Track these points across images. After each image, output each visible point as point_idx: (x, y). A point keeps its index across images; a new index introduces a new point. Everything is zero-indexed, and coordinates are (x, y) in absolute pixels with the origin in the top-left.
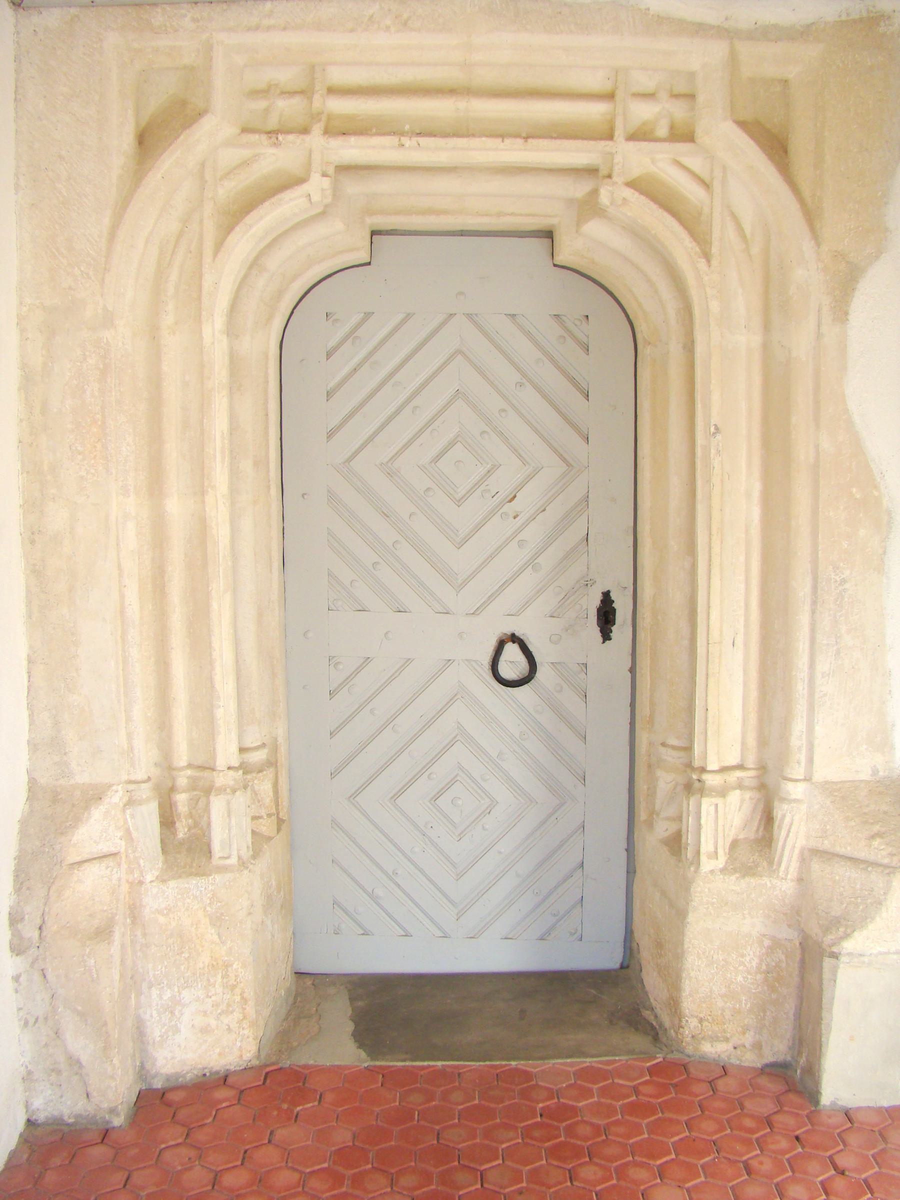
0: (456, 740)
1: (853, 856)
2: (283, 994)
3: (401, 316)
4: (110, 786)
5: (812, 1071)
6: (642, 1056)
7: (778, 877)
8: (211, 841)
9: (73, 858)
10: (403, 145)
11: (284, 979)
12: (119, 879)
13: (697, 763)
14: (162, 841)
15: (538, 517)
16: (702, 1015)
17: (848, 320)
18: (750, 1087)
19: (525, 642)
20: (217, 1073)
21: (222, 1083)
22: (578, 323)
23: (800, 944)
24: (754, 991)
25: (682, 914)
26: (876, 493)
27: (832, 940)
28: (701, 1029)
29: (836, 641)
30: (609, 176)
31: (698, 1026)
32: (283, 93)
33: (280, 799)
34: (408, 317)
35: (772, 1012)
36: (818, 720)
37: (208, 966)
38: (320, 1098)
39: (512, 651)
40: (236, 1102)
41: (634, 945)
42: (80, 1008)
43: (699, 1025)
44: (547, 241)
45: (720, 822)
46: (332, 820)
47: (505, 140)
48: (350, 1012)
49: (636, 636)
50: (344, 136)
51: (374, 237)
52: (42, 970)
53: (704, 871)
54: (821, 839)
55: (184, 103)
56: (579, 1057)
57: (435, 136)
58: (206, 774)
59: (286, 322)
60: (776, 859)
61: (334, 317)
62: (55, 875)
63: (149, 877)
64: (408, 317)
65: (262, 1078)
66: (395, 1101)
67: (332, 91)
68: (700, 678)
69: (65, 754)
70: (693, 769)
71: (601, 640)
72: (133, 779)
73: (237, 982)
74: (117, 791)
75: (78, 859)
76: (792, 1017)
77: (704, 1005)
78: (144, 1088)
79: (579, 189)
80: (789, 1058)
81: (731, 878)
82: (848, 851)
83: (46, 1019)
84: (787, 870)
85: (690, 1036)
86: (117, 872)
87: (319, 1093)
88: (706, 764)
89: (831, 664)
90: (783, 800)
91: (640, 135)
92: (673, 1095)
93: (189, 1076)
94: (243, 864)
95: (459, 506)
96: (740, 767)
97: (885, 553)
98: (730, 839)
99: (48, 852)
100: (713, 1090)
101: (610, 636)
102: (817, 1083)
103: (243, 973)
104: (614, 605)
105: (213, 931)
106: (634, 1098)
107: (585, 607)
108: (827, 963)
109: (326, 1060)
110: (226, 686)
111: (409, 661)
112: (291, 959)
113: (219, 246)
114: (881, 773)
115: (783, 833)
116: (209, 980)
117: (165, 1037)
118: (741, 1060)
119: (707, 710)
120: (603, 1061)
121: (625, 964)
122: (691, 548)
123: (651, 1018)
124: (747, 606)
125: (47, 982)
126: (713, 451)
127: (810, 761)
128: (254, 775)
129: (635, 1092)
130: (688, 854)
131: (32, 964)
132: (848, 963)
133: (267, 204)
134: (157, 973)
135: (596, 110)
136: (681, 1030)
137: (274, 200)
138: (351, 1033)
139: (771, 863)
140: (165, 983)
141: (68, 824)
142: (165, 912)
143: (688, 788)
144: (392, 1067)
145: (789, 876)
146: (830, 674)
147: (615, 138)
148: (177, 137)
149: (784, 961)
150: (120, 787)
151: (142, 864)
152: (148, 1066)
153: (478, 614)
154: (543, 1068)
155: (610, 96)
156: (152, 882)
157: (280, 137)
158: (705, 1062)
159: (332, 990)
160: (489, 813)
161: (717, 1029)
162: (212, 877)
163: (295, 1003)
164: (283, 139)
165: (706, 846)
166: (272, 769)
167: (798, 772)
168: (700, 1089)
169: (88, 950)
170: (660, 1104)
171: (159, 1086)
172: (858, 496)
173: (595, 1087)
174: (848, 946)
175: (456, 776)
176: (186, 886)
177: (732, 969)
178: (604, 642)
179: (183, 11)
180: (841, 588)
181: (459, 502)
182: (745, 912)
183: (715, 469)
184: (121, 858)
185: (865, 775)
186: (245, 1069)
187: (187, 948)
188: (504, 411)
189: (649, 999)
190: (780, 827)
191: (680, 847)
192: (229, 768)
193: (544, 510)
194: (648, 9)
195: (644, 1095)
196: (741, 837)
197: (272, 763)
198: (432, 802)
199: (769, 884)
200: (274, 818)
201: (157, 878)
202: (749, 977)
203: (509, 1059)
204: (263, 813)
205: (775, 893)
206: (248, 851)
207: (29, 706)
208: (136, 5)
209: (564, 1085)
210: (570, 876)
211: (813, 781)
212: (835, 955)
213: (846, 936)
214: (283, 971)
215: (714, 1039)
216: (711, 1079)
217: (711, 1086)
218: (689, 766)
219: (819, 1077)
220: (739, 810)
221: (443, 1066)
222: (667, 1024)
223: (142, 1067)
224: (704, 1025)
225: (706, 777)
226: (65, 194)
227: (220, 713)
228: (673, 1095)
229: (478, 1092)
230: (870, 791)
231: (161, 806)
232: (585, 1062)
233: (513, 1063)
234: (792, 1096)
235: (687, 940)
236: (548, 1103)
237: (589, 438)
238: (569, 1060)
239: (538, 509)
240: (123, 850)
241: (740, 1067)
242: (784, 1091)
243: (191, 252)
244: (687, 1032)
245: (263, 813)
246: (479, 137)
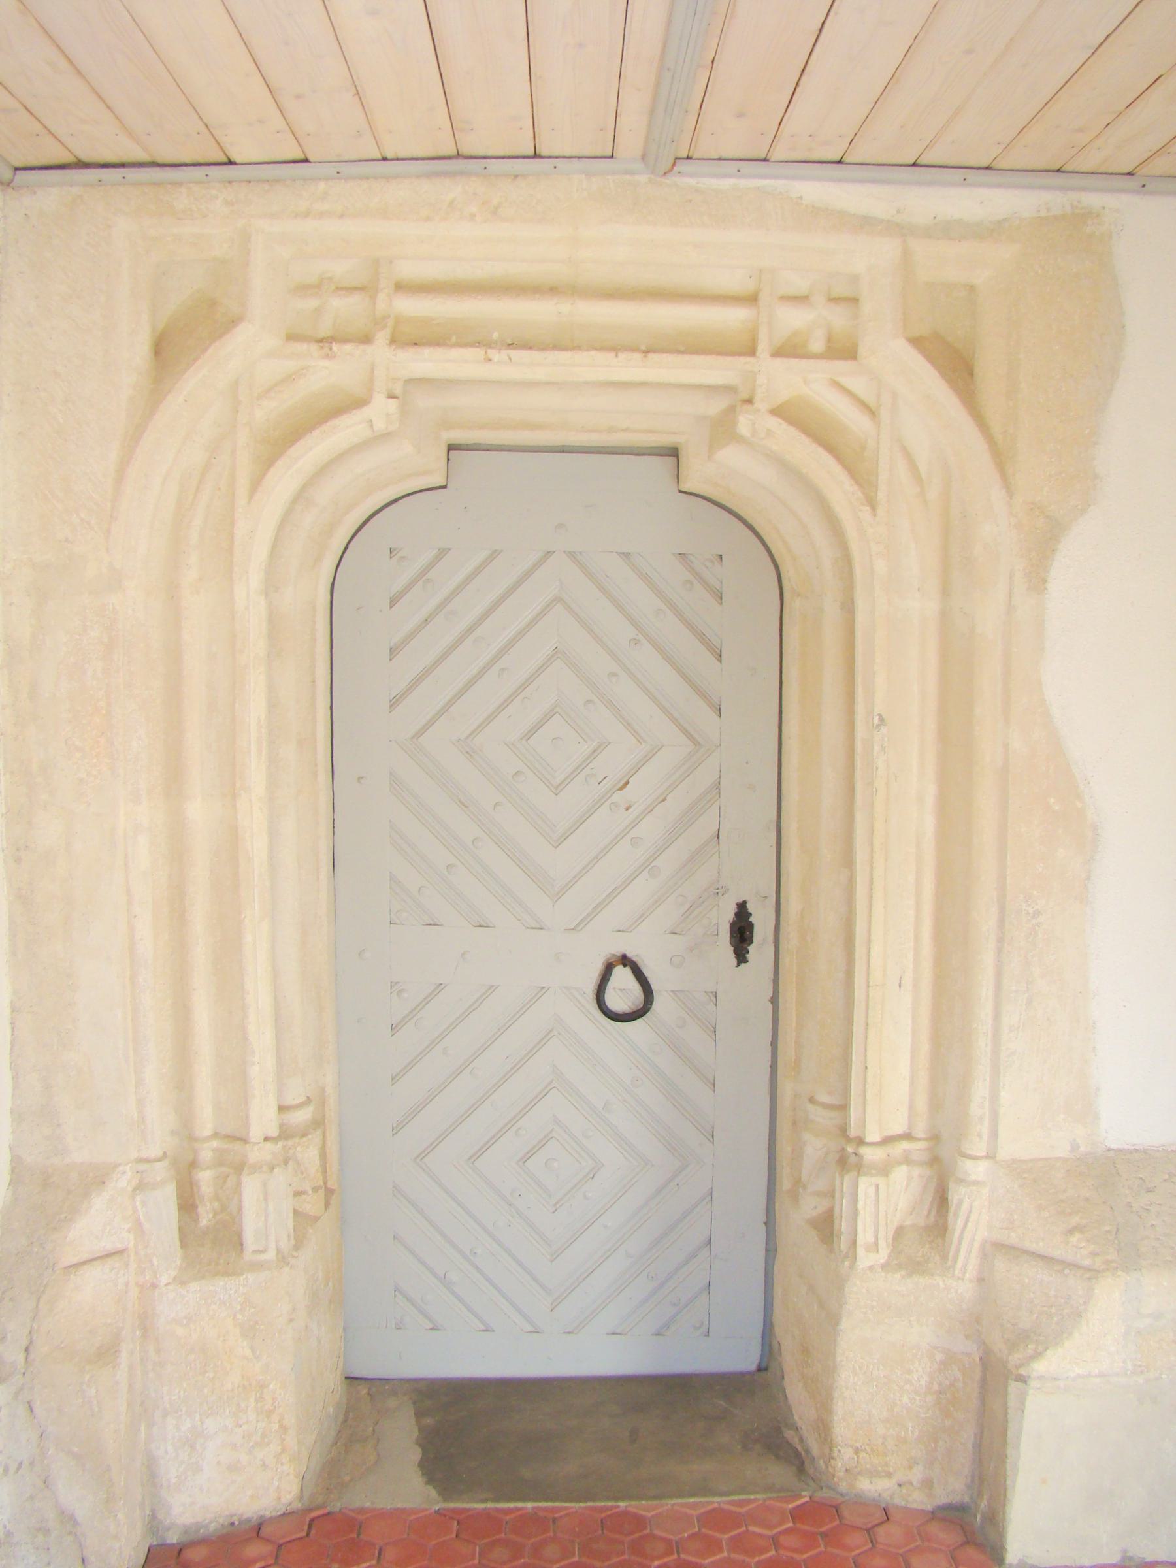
0: (550, 1136)
1: (1046, 1254)
2: (331, 1413)
3: (484, 555)
4: (116, 1166)
5: (995, 1519)
6: (782, 1494)
7: (953, 1276)
8: (242, 1231)
9: (70, 1258)
10: (490, 360)
11: (333, 1392)
12: (127, 1284)
13: (853, 1132)
14: (181, 1229)
15: (655, 809)
16: (858, 1445)
17: (1046, 589)
18: (917, 1537)
19: (639, 965)
20: (249, 1520)
21: (255, 1534)
22: (709, 564)
23: (981, 1359)
24: (923, 1416)
25: (834, 1319)
26: (1079, 805)
27: (1019, 1359)
28: (858, 1462)
29: (1027, 988)
30: (749, 401)
31: (853, 1459)
32: (338, 289)
33: (328, 1165)
34: (495, 554)
35: (946, 1442)
36: (1004, 1085)
37: (238, 1387)
38: (380, 1553)
39: (622, 977)
40: (274, 1561)
41: (776, 1347)
42: (76, 1449)
43: (855, 1457)
44: (671, 460)
45: (882, 1207)
46: (394, 1187)
47: (620, 354)
48: (416, 1434)
49: (779, 958)
50: (416, 346)
51: (451, 452)
52: (29, 1402)
53: (861, 1267)
54: (1007, 1231)
55: (213, 304)
56: (705, 1496)
57: (531, 348)
58: (238, 1146)
59: (338, 559)
60: (951, 1254)
61: (400, 555)
62: (45, 1283)
63: (164, 1279)
64: (495, 554)
65: (306, 1528)
66: (473, 1558)
67: (401, 287)
68: (858, 1028)
69: (59, 1125)
70: (849, 1140)
71: (735, 961)
72: (145, 1157)
73: (275, 1407)
74: (125, 1173)
75: (75, 1260)
76: (970, 1446)
77: (861, 1432)
78: (155, 1543)
79: (714, 407)
80: (967, 1499)
81: (896, 1276)
82: (1040, 1247)
83: (32, 1464)
84: (965, 1268)
85: (844, 1469)
86: (124, 1275)
87: (378, 1547)
88: (865, 1134)
89: (1021, 1015)
90: (961, 1181)
91: (790, 350)
92: (822, 1548)
93: (212, 1527)
94: (283, 1259)
95: (557, 795)
96: (907, 1136)
97: (1088, 878)
98: (895, 1224)
99: (37, 1253)
100: (872, 1542)
101: (746, 958)
102: (1001, 1536)
103: (282, 1395)
104: (751, 919)
105: (245, 1343)
106: (773, 1552)
107: (714, 922)
108: (1013, 1387)
109: (385, 1502)
110: (262, 1037)
111: (492, 988)
112: (341, 1364)
113: (256, 484)
114: (1082, 1149)
115: (960, 1222)
116: (238, 1405)
117: (183, 1477)
118: (907, 1501)
119: (866, 1067)
120: (733, 1501)
121: (764, 1365)
122: (848, 859)
123: (796, 1442)
124: (917, 938)
125: (35, 1417)
126: (876, 748)
127: (994, 1134)
128: (297, 1140)
129: (774, 1544)
130: (841, 1245)
131: (16, 1395)
132: (1039, 1388)
133: (317, 432)
134: (174, 1398)
135: (734, 317)
136: (832, 1461)
137: (326, 427)
138: (417, 1464)
139: (944, 1258)
140: (184, 1409)
141: (63, 1216)
142: (185, 1322)
143: (843, 1162)
144: (469, 1510)
145: (967, 1275)
146: (1019, 1028)
147: (758, 354)
148: (206, 350)
149: (961, 1378)
150: (128, 1168)
151: (156, 1263)
152: (161, 1515)
153: (581, 930)
154: (659, 1510)
155: (752, 299)
156: (167, 1284)
157: (335, 347)
158: (861, 1502)
159: (392, 1403)
160: (593, 1178)
161: (877, 1462)
162: (244, 1276)
163: (345, 1421)
164: (338, 350)
165: (864, 1236)
166: (319, 1132)
167: (979, 1147)
168: (856, 1540)
169: (87, 1377)
170: (804, 1560)
171: (175, 1541)
172: (1057, 808)
173: (725, 1537)
174: (1039, 1367)
175: (551, 1132)
176: (211, 1288)
177: (896, 1388)
178: (738, 965)
179: (214, 192)
180: (1034, 921)
181: (557, 789)
182: (912, 1319)
183: (879, 770)
184: (129, 1256)
185: (1063, 1151)
186: (284, 1514)
187: (212, 1366)
188: (615, 675)
189: (793, 1415)
190: (956, 1215)
191: (832, 1233)
192: (266, 1139)
193: (664, 800)
194: (801, 198)
195: (786, 1548)
196: (908, 1223)
197: (318, 1123)
198: (521, 1163)
199: (942, 1285)
200: (322, 1193)
201: (175, 1278)
202: (918, 1398)
203: (616, 1499)
204: (307, 1186)
205: (949, 1296)
206: (289, 1240)
207: (13, 1066)
208: (155, 184)
209: (686, 1535)
210: (693, 1256)
211: (998, 1159)
212: (1022, 1378)
213: (1037, 1355)
214: (332, 1381)
215: (873, 1474)
216: (870, 1525)
217: (869, 1535)
218: (843, 1130)
219: (1003, 1529)
220: (906, 1189)
221: (534, 1508)
222: (815, 1451)
223: (153, 1516)
224: (861, 1456)
225: (863, 1150)
226: (61, 421)
227: (254, 1071)
228: (822, 1548)
229: (579, 1544)
230: (1068, 1171)
231: (180, 1187)
232: (713, 1502)
233: (622, 1504)
234: (971, 1551)
235: (839, 1351)
236: (666, 1560)
237: (722, 709)
238: (692, 1500)
239: (658, 798)
240: (131, 1245)
241: (906, 1510)
242: (960, 1543)
243: (219, 489)
244: (840, 1464)
245: (307, 1186)
246: (588, 350)
